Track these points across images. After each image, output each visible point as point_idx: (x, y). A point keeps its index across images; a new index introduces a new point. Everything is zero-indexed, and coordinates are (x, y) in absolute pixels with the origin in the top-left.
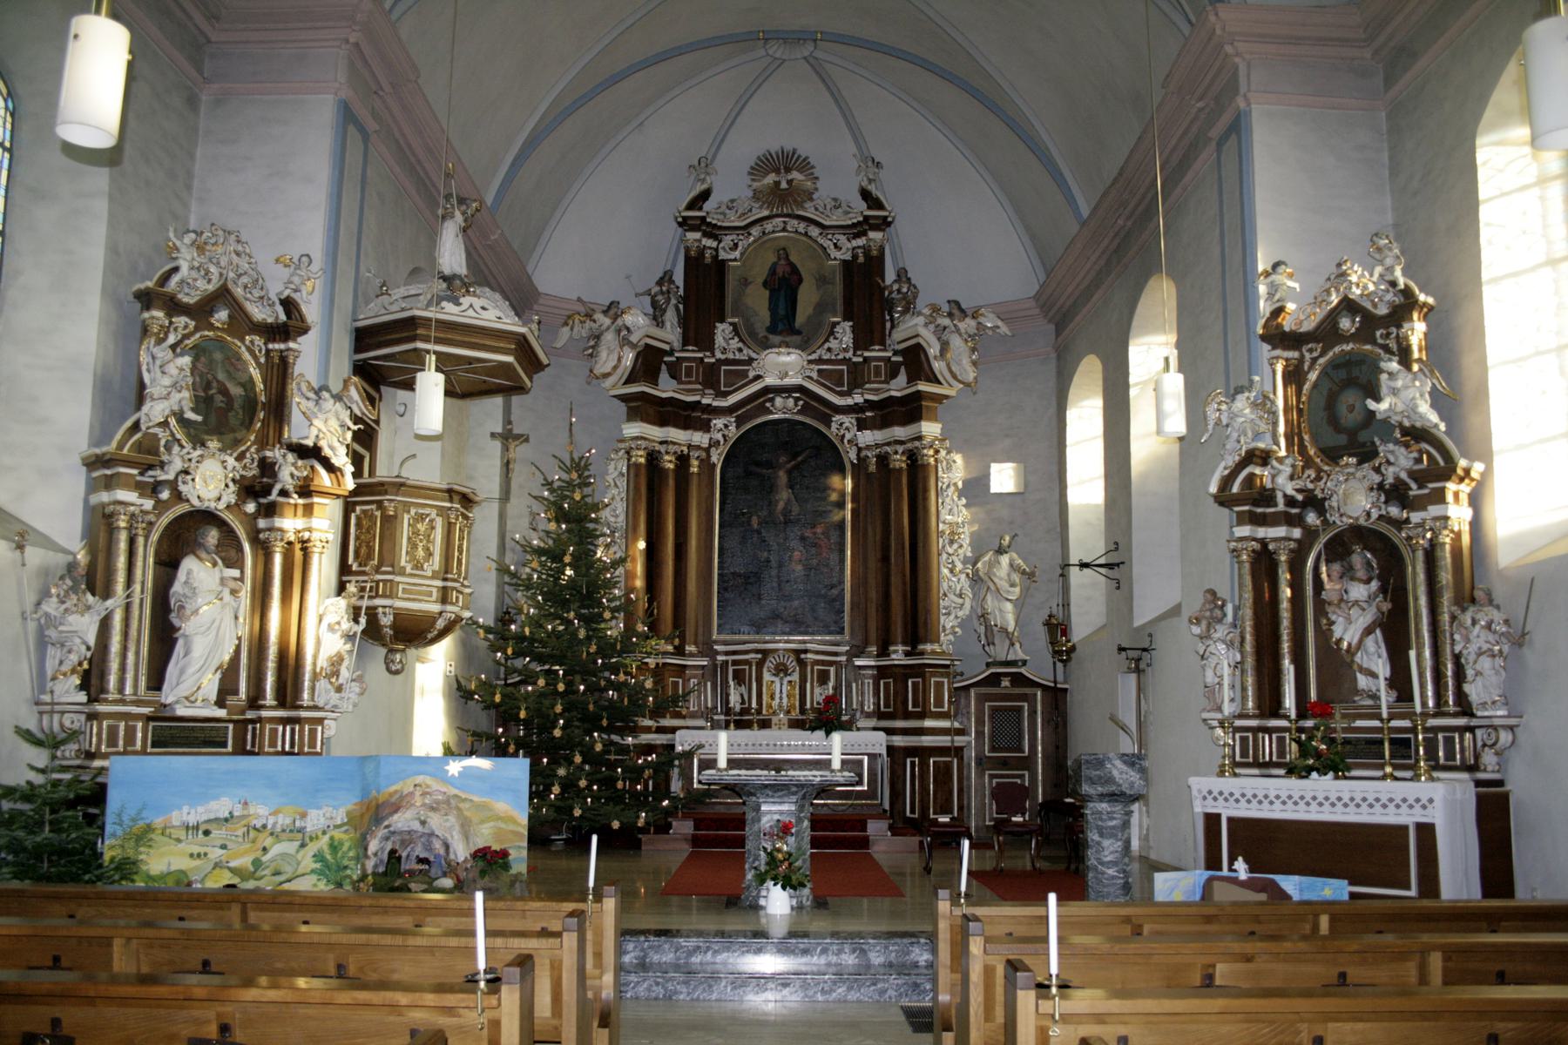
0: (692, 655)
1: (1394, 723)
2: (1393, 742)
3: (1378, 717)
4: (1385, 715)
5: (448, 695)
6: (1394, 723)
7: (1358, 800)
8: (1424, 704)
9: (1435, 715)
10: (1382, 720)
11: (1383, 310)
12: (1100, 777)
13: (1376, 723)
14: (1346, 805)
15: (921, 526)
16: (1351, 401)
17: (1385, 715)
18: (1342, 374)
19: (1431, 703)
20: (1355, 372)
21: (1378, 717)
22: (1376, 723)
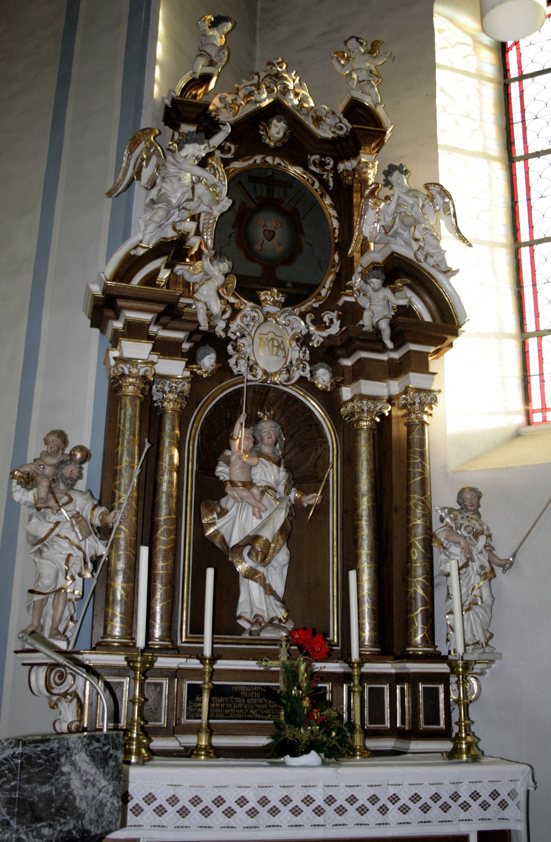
0: (289, 287)
1: (221, 664)
2: (216, 691)
3: (199, 655)
4: (208, 652)
5: (338, 764)
6: (221, 664)
7: (363, 800)
8: (149, 636)
9: (165, 651)
10: (202, 659)
11: (325, 132)
12: (48, 799)
13: (194, 663)
14: (319, 811)
15: (504, 112)
16: (271, 225)
17: (208, 652)
18: (262, 191)
19: (157, 632)
20: (278, 193)
21: (199, 655)
22: (194, 663)
